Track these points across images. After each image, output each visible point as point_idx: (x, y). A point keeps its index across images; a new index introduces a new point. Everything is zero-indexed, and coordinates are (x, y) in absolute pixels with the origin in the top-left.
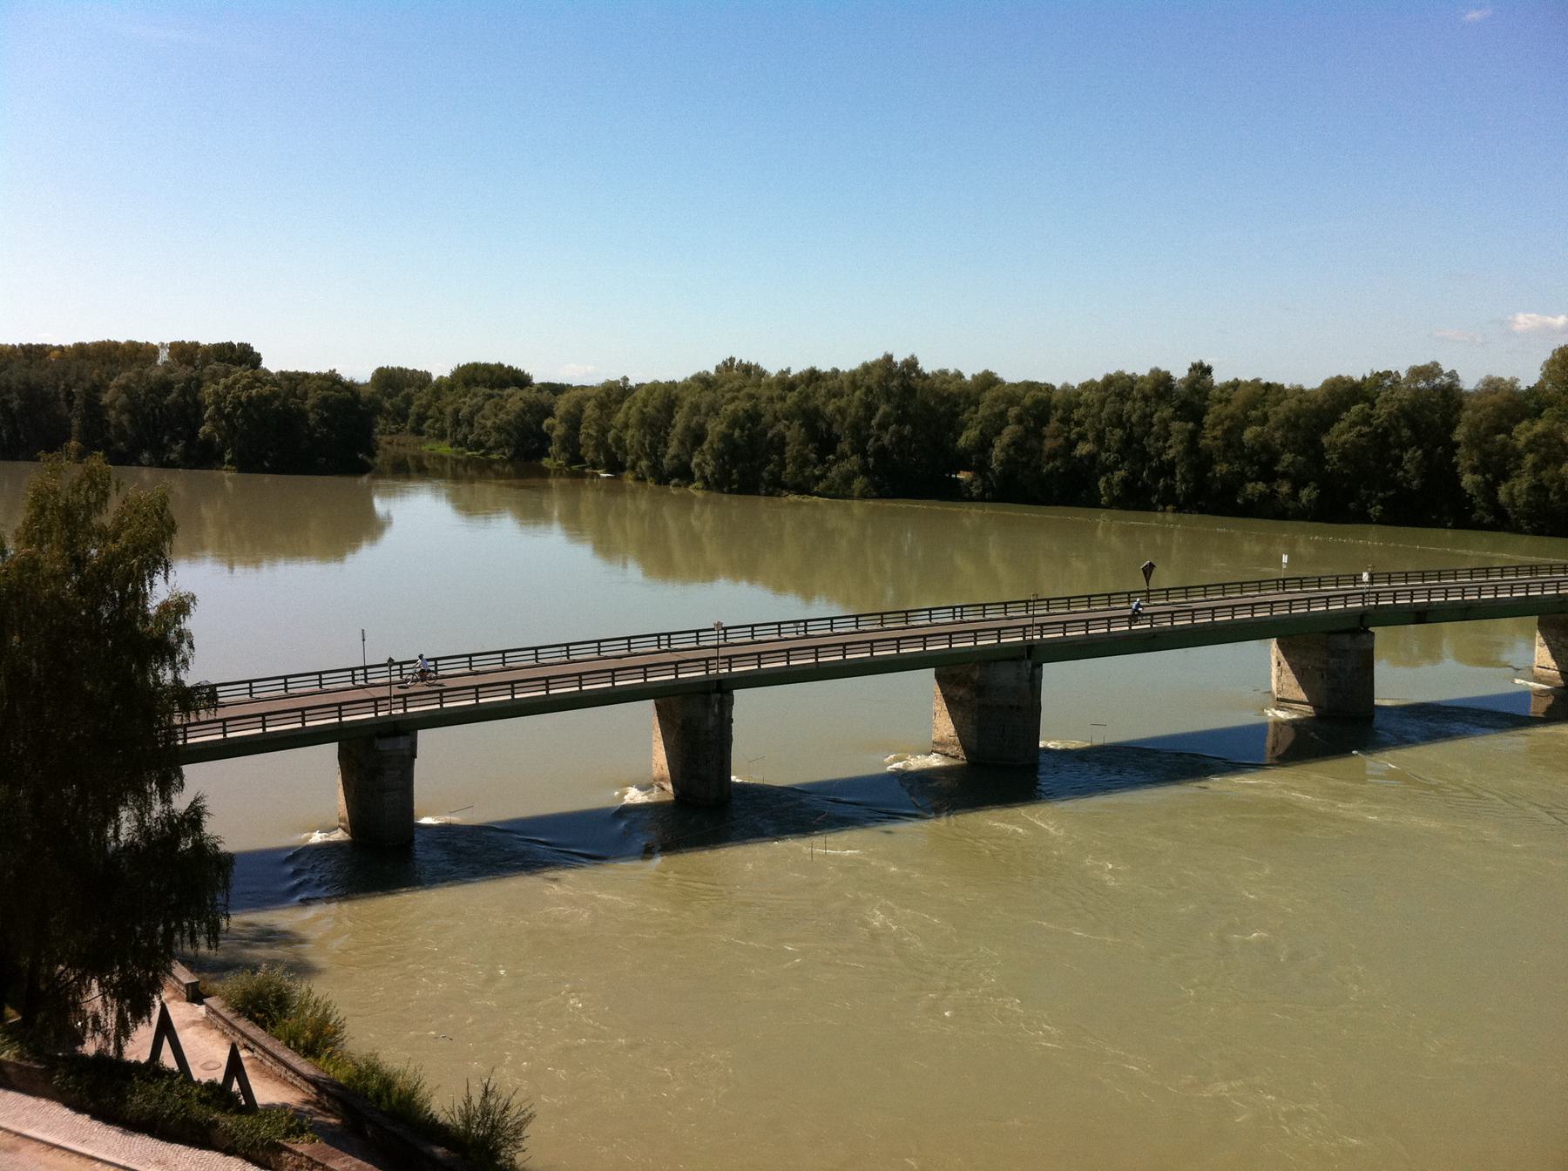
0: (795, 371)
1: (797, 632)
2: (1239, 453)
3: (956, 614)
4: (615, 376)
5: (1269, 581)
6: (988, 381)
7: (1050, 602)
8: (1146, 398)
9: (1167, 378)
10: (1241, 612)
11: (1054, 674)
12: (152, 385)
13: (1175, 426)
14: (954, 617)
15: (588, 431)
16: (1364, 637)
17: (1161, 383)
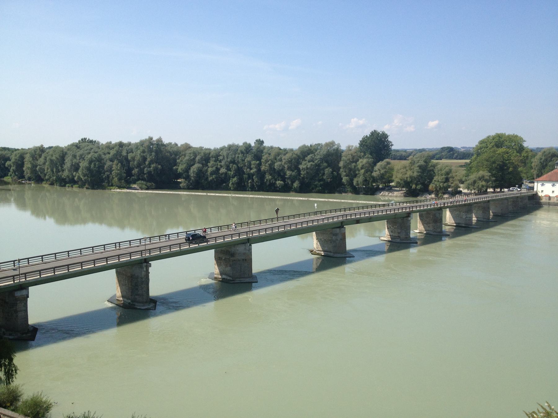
0: (113, 142)
1: (166, 239)
3: (117, 246)
4: (38, 145)
6: (187, 147)
7: (222, 227)
8: (242, 152)
9: (250, 145)
10: (227, 238)
11: (256, 248)
13: (253, 162)
14: (219, 230)
15: (27, 166)
16: (343, 229)
17: (248, 148)
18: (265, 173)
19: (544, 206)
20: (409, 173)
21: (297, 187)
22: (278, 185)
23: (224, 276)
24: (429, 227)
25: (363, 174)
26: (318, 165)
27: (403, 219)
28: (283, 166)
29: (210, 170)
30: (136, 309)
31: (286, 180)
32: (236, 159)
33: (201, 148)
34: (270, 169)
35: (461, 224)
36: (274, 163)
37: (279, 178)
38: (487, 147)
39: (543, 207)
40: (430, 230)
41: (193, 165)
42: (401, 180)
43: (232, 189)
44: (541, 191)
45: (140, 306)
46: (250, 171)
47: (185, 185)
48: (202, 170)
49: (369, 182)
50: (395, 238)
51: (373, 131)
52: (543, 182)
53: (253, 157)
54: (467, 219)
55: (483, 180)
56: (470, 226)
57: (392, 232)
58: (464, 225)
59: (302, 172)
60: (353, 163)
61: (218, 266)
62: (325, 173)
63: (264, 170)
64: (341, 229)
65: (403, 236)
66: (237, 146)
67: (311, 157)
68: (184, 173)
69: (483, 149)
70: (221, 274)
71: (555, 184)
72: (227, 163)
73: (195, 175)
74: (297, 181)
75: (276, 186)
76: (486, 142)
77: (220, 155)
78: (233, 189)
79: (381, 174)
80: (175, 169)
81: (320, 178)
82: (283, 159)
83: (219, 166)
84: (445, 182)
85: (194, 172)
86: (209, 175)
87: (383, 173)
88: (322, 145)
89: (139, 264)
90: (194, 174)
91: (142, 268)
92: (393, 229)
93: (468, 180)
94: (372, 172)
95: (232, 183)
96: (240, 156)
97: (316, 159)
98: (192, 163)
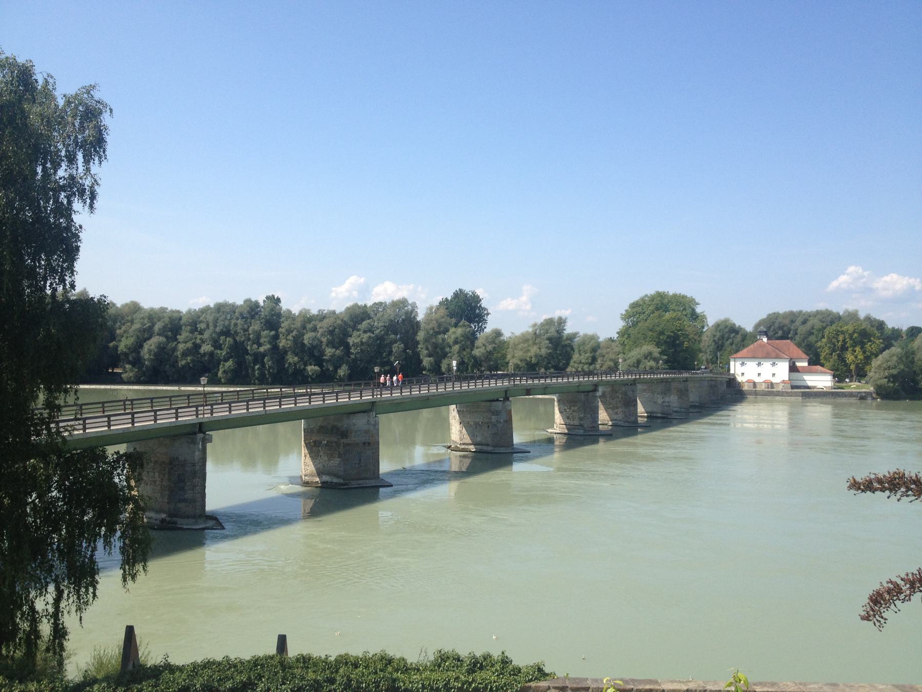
2: (739, 346)
5: (142, 399)
9: (256, 304)
12: (777, 321)
17: (252, 309)
18: (286, 352)
19: (748, 396)
20: (534, 350)
21: (344, 375)
22: (310, 373)
23: (326, 478)
24: (616, 413)
25: (458, 353)
26: (380, 338)
27: (588, 395)
28: (318, 340)
29: (182, 348)
30: (182, 529)
31: (324, 364)
32: (231, 328)
33: (163, 310)
34: (294, 345)
35: (655, 413)
36: (303, 335)
37: (311, 361)
38: (644, 313)
39: (747, 397)
40: (618, 418)
41: (149, 339)
42: (521, 361)
43: (223, 382)
44: (740, 375)
45: (188, 525)
46: (258, 348)
47: (131, 374)
48: (165, 348)
49: (468, 366)
50: (574, 429)
51: (458, 290)
52: (743, 360)
53: (264, 325)
54: (664, 404)
55: (651, 358)
56: (669, 417)
57: (568, 418)
58: (659, 415)
59: (352, 351)
60: (440, 334)
61: (312, 458)
62: (392, 351)
63: (284, 347)
64: (506, 403)
65: (587, 424)
66: (233, 306)
67: (369, 324)
68: (131, 352)
69: (638, 315)
70: (320, 473)
71: (762, 363)
72: (213, 336)
73: (152, 357)
74: (344, 365)
75: (306, 374)
76: (640, 305)
77: (201, 322)
78: (226, 381)
79: (487, 351)
80: (113, 346)
81: (385, 360)
82: (318, 327)
83: (198, 341)
84: (591, 364)
85: (150, 351)
86: (179, 356)
87: (490, 351)
88: (386, 305)
89: (189, 434)
90: (150, 355)
91: (194, 442)
92: (570, 413)
93: (628, 359)
94: (472, 350)
95: (225, 372)
96: (239, 321)
97: (377, 328)
98: (146, 336)
